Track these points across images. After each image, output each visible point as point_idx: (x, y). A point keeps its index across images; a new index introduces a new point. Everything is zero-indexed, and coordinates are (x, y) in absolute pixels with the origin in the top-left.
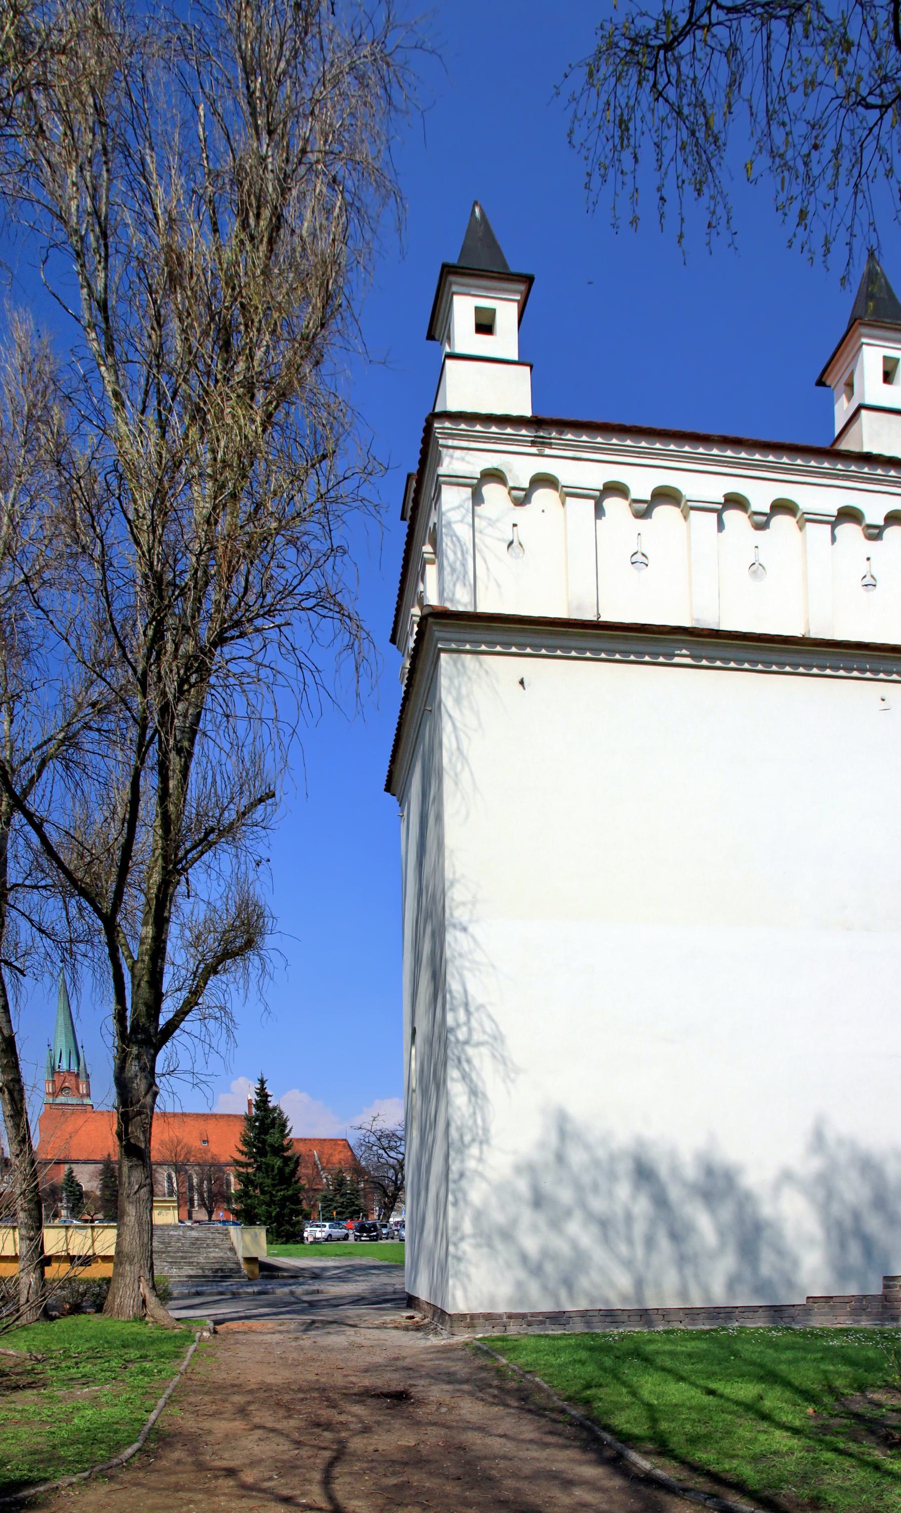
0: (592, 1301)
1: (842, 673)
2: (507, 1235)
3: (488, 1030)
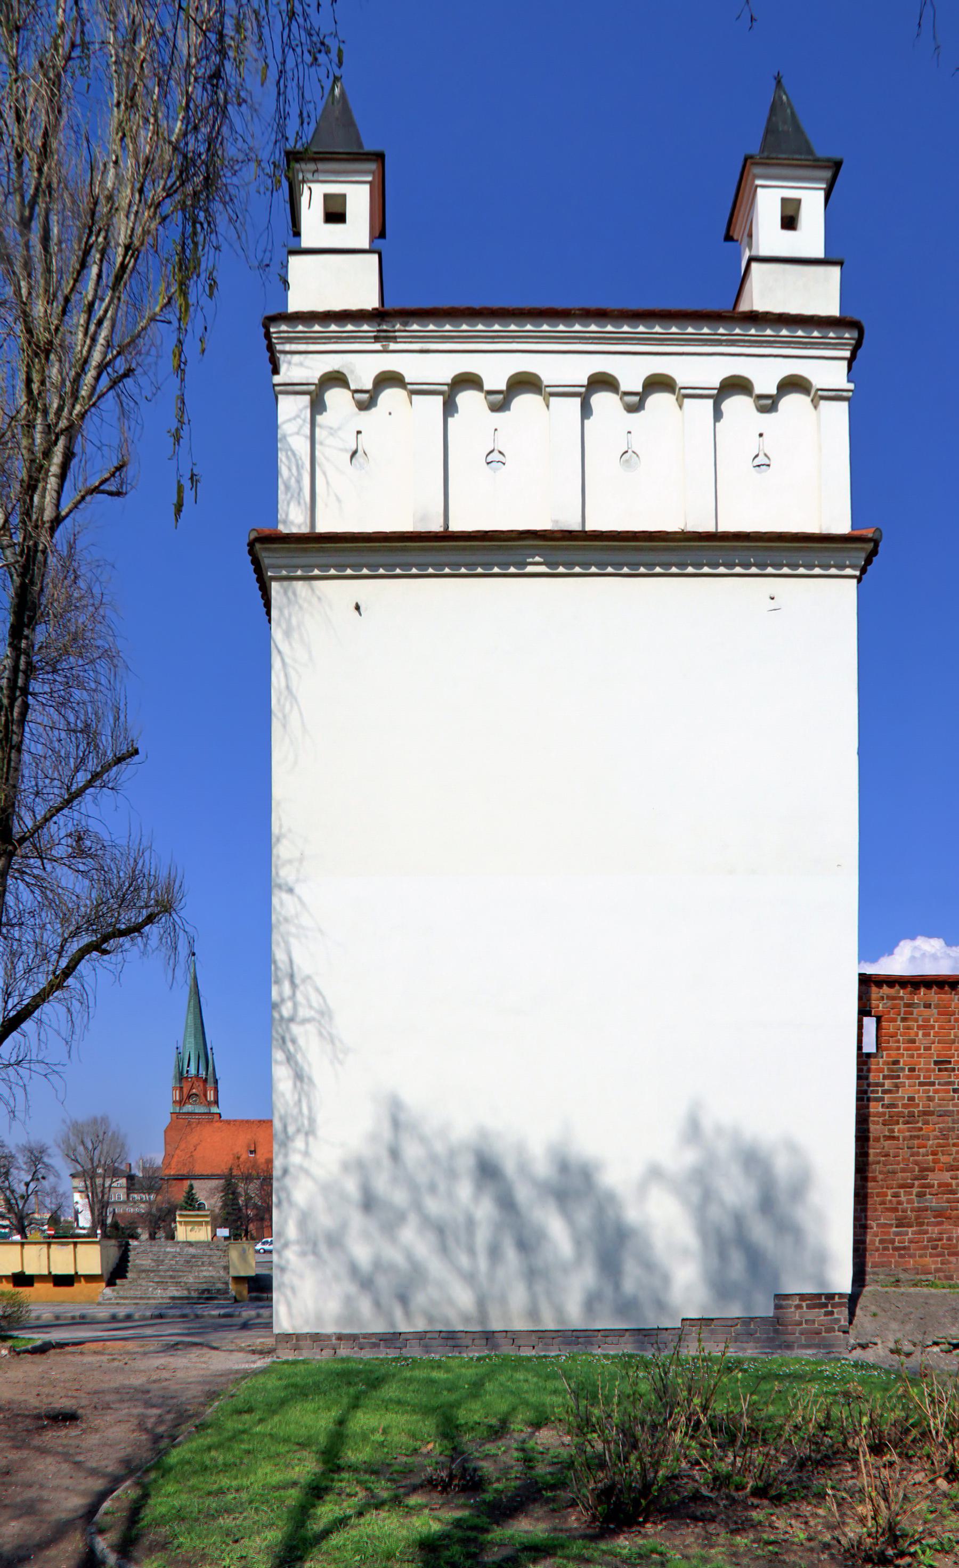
0: (431, 1319)
1: (722, 570)
2: (335, 1241)
3: (315, 1004)
